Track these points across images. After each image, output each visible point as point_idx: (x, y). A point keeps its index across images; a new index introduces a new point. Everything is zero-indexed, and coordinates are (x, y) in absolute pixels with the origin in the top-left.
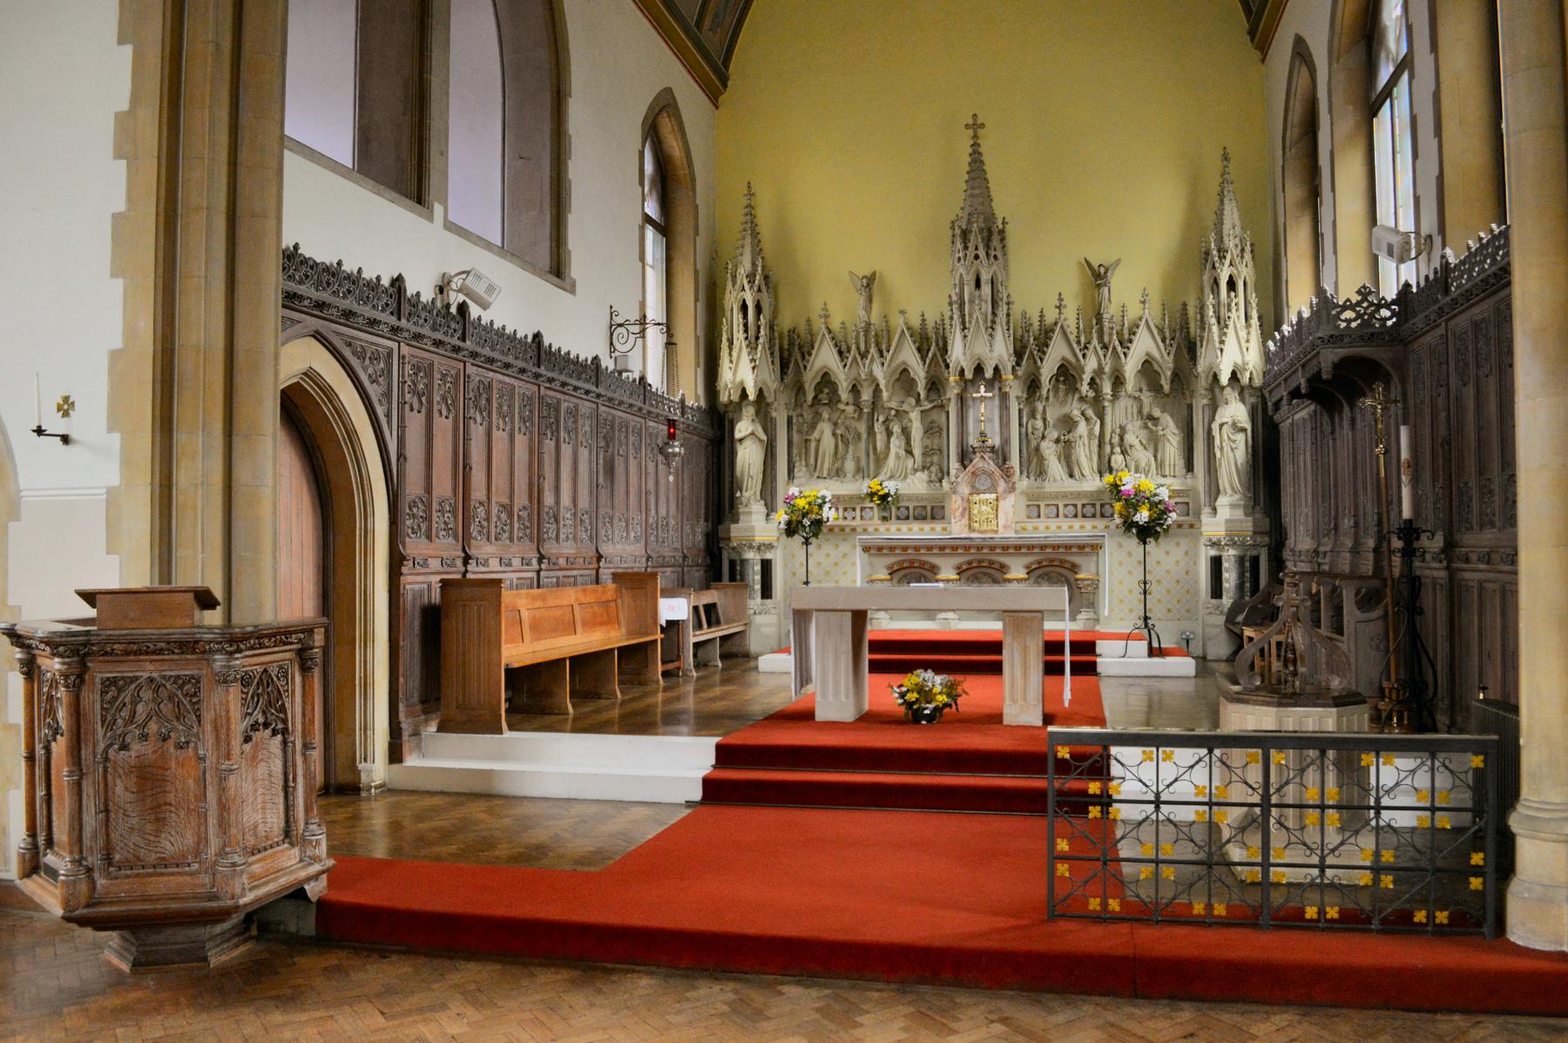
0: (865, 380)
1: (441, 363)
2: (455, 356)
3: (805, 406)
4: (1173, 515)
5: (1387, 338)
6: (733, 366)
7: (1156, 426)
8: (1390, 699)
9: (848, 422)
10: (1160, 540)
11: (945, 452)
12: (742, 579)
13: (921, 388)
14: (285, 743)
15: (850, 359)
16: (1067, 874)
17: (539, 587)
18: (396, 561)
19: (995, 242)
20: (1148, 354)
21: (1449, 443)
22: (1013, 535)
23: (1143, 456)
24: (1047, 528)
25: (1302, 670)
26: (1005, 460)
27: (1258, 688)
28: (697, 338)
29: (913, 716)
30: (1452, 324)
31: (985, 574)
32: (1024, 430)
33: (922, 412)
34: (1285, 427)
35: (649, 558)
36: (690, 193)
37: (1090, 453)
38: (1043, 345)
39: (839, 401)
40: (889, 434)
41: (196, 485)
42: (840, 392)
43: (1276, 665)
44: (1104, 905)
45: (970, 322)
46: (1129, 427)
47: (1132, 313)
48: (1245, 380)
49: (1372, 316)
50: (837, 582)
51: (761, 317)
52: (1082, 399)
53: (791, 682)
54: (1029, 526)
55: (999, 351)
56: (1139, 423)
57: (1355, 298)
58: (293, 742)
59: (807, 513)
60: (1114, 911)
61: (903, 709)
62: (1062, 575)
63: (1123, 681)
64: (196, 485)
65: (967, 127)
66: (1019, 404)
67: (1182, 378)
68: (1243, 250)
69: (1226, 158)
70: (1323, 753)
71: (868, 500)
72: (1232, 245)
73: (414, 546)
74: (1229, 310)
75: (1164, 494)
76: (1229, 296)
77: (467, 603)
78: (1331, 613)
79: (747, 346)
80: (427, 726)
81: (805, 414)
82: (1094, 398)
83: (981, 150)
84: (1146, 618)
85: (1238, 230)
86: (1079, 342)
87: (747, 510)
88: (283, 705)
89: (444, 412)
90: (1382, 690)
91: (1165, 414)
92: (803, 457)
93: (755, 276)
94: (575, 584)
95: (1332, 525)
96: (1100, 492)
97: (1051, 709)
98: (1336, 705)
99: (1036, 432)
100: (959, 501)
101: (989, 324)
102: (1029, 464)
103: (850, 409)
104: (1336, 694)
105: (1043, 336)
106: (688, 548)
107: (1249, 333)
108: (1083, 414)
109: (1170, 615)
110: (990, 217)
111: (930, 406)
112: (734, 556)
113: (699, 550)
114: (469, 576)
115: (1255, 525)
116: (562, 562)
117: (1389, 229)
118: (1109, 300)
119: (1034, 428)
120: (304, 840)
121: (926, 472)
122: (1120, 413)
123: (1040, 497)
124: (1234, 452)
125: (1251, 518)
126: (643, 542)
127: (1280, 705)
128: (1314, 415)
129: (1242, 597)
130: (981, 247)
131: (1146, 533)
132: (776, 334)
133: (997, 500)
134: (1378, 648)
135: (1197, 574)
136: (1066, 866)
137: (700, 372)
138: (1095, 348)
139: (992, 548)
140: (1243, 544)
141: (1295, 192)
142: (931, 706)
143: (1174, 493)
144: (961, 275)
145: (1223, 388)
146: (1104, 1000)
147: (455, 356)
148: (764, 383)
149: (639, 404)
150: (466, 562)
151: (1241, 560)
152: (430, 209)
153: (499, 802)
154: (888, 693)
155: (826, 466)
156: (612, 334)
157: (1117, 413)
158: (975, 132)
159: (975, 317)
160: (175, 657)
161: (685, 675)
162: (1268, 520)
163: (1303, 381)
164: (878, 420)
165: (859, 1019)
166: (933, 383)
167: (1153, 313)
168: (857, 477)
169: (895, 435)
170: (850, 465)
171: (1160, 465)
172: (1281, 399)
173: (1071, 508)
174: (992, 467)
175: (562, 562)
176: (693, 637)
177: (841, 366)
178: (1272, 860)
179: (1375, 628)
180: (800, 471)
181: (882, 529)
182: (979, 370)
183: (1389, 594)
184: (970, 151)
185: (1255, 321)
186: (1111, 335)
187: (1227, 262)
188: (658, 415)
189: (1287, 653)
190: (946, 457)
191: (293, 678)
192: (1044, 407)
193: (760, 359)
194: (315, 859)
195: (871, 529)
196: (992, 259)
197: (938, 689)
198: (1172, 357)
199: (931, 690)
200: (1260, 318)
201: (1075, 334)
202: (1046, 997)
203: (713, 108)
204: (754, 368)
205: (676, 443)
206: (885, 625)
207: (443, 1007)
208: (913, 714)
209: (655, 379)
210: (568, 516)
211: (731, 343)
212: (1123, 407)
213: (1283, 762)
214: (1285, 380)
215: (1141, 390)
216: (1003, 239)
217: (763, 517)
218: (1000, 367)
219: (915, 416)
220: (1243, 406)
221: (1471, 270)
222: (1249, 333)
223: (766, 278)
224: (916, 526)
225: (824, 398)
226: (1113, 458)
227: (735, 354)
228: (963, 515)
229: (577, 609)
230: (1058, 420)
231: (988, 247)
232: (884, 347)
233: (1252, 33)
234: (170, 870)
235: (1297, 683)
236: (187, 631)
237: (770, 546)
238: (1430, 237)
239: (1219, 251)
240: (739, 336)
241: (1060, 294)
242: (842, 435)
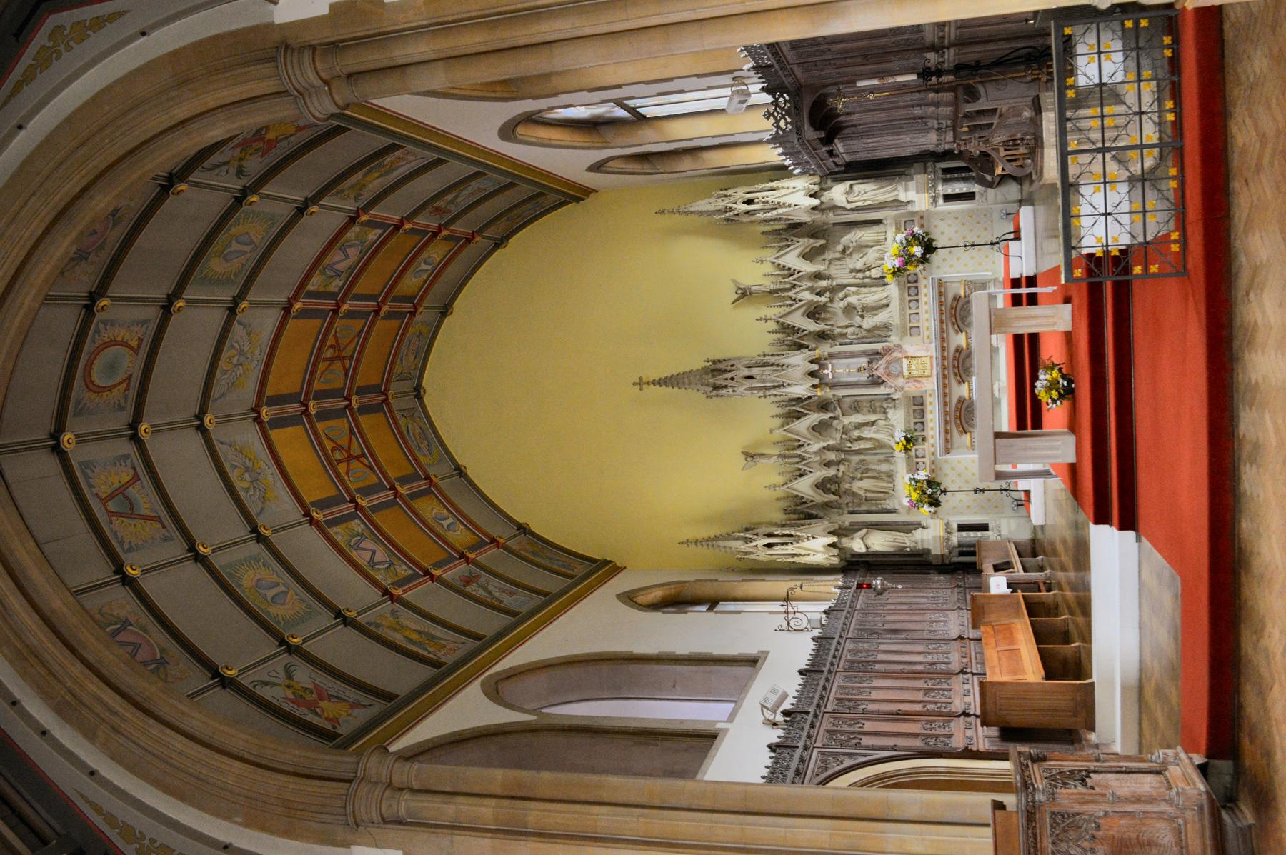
1: (826, 724)
2: (820, 717)
3: (841, 501)
4: (916, 229)
5: (797, 99)
6: (812, 553)
7: (849, 247)
8: (1038, 74)
10: (934, 238)
11: (873, 397)
12: (974, 546)
13: (826, 416)
14: (1095, 772)
15: (806, 468)
16: (1157, 266)
17: (985, 674)
18: (968, 754)
19: (720, 366)
21: (867, 56)
22: (933, 345)
23: (872, 255)
24: (927, 320)
25: (1019, 136)
26: (877, 353)
27: (1033, 161)
29: (1068, 393)
30: (791, 62)
31: (963, 364)
32: (855, 341)
34: (848, 158)
35: (960, 608)
36: (687, 584)
38: (793, 330)
39: (836, 476)
40: (860, 438)
41: (922, 839)
43: (1022, 150)
44: (1175, 242)
45: (778, 381)
46: (851, 266)
47: (768, 268)
48: (816, 188)
49: (782, 109)
50: (973, 474)
52: (831, 301)
53: (1050, 480)
54: (926, 333)
55: (799, 360)
56: (848, 260)
57: (772, 120)
58: (1095, 767)
59: (922, 491)
60: (1179, 235)
61: (1065, 402)
62: (963, 307)
63: (1039, 255)
64: (922, 839)
67: (814, 231)
68: (725, 196)
69: (663, 212)
70: (1068, 120)
71: (910, 452)
72: (723, 204)
73: (958, 743)
74: (767, 202)
75: (901, 237)
76: (758, 203)
77: (998, 707)
78: (982, 118)
79: (798, 542)
80: (1091, 740)
81: (847, 501)
82: (831, 293)
83: (657, 379)
84: (992, 244)
85: (712, 200)
86: (791, 305)
88: (1069, 771)
89: (861, 725)
90: (1033, 80)
93: (746, 538)
94: (982, 654)
95: (920, 121)
96: (899, 284)
97: (1060, 297)
98: (1041, 112)
100: (908, 385)
101: (780, 368)
103: (842, 468)
104: (1033, 113)
105: (787, 331)
106: (951, 584)
107: (783, 188)
108: (842, 300)
110: (705, 371)
111: (839, 409)
112: (956, 552)
113: (952, 578)
114: (978, 713)
115: (920, 173)
116: (965, 660)
117: (730, 100)
119: (854, 334)
120: (1163, 763)
122: (841, 274)
124: (868, 192)
125: (915, 176)
126: (947, 612)
127: (1042, 147)
128: (842, 140)
129: (973, 178)
130: (725, 376)
131: (929, 248)
132: (788, 522)
133: (907, 357)
134: (1006, 85)
135: (957, 211)
136: (1151, 267)
137: (816, 578)
139: (944, 358)
140: (933, 180)
141: (686, 164)
142: (1061, 381)
143: (898, 230)
144: (745, 389)
145: (822, 203)
146: (1232, 237)
147: (820, 717)
148: (824, 530)
149: (844, 613)
150: (968, 715)
151: (946, 181)
152: (720, 730)
153: (1144, 676)
154: (1055, 413)
155: (885, 485)
156: (795, 630)
157: (840, 275)
158: (644, 383)
159: (775, 379)
160: (1038, 826)
161: (1049, 578)
162: (915, 164)
163: (824, 149)
165: (1253, 382)
166: (822, 408)
167: (770, 255)
170: (884, 467)
171: (878, 243)
172: (834, 162)
173: (911, 304)
174: (883, 362)
175: (965, 660)
176: (1019, 573)
177: (810, 475)
178: (1139, 143)
179: (991, 89)
180: (889, 504)
181: (932, 441)
182: (812, 374)
183: (968, 82)
184: (658, 386)
185: (774, 184)
186: (785, 283)
187: (734, 206)
188: (852, 601)
189: (1011, 144)
190: (876, 397)
191: (1050, 765)
192: (838, 327)
193: (806, 533)
194: (1176, 755)
195: (932, 450)
196: (734, 368)
197: (1048, 377)
199: (1049, 381)
200: (772, 181)
201: (785, 308)
202: (1234, 271)
203: (625, 571)
204: (813, 538)
205: (874, 583)
206: (1005, 421)
207: (1266, 650)
208: (1068, 394)
209: (825, 606)
210: (930, 657)
211: (794, 555)
212: (837, 272)
213: (1076, 142)
214: (822, 160)
215: (824, 260)
216: (719, 361)
217: (925, 531)
218: (810, 359)
219: (846, 420)
220: (834, 188)
221: (760, 54)
222: (783, 188)
223: (747, 530)
224: (929, 416)
225: (834, 487)
226: (873, 276)
227: (803, 552)
228: (919, 382)
229: (999, 649)
230: (847, 317)
231: (726, 371)
232: (797, 444)
233: (578, 200)
234: (1183, 838)
235: (1028, 137)
236: (1020, 815)
237: (947, 525)
238: (734, 78)
239: (726, 212)
240: (790, 549)
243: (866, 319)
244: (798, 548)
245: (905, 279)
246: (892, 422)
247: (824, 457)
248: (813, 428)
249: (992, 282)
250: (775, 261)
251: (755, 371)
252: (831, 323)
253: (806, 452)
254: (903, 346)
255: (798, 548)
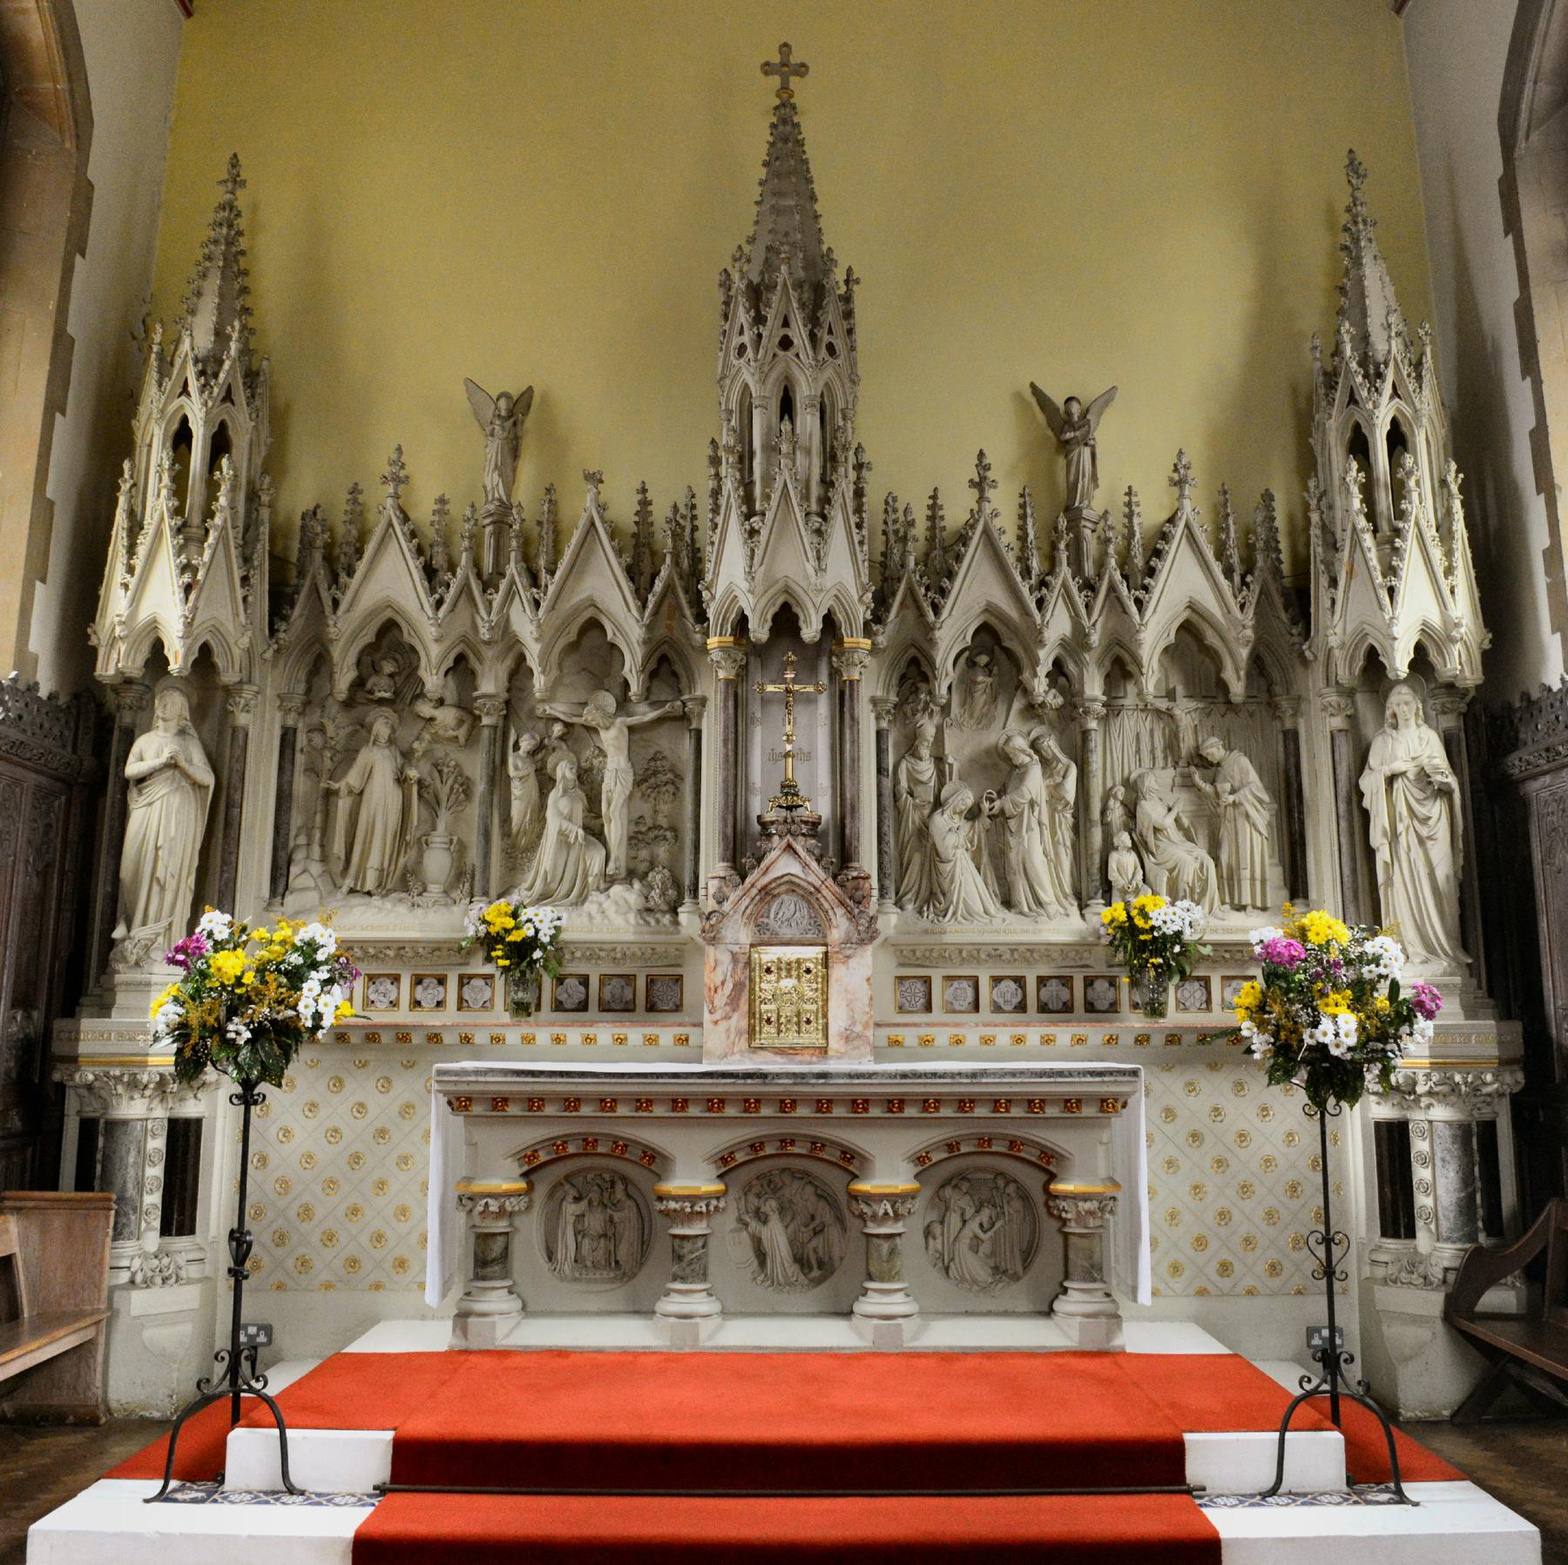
0: (488, 643)
3: (333, 709)
9: (440, 751)
11: (688, 837)
12: (107, 1184)
13: (632, 669)
19: (831, 314)
20: (1192, 606)
23: (1189, 857)
28: (43, 509)
32: (888, 783)
33: (631, 729)
37: (1055, 844)
39: (420, 695)
40: (545, 783)
42: (422, 673)
45: (767, 497)
46: (1150, 782)
47: (1150, 514)
51: (224, 462)
52: (1032, 711)
54: (910, 1037)
62: (1010, 1180)
65: (767, 69)
66: (878, 718)
86: (1026, 572)
87: (137, 976)
91: (1236, 753)
92: (317, 835)
93: (221, 363)
96: (1082, 946)
99: (919, 790)
100: (725, 959)
101: (814, 507)
102: (903, 870)
103: (447, 717)
108: (1034, 745)
109: (1275, 1283)
111: (652, 715)
118: (1094, 478)
119: (914, 780)
121: (637, 885)
123: (942, 955)
133: (826, 961)
138: (1065, 586)
139: (823, 1104)
148: (216, 630)
151: (1463, 1133)
155: (374, 861)
159: (778, 485)
164: (516, 747)
166: (664, 659)
167: (1195, 508)
168: (456, 894)
169: (559, 786)
170: (437, 863)
171: (1229, 881)
174: (816, 875)
180: (308, 871)
181: (513, 1037)
182: (786, 621)
187: (1387, 389)
192: (940, 731)
195: (481, 1038)
196: (823, 353)
198: (1250, 611)
204: (188, 589)
211: (135, 527)
212: (1130, 736)
218: (840, 617)
219: (612, 739)
223: (251, 377)
226: (1114, 858)
228: (733, 1001)
231: (813, 321)
239: (1363, 363)
240: (158, 505)
241: (981, 455)
242: (420, 782)
243: (966, 826)
244: (158, 534)
245: (1100, 969)
246: (595, 896)
247: (489, 653)
248: (593, 626)
249: (1106, 1306)
250: (1181, 525)
251: (807, 422)
252: (955, 709)
253: (511, 594)
254: (869, 949)
255: (158, 534)
